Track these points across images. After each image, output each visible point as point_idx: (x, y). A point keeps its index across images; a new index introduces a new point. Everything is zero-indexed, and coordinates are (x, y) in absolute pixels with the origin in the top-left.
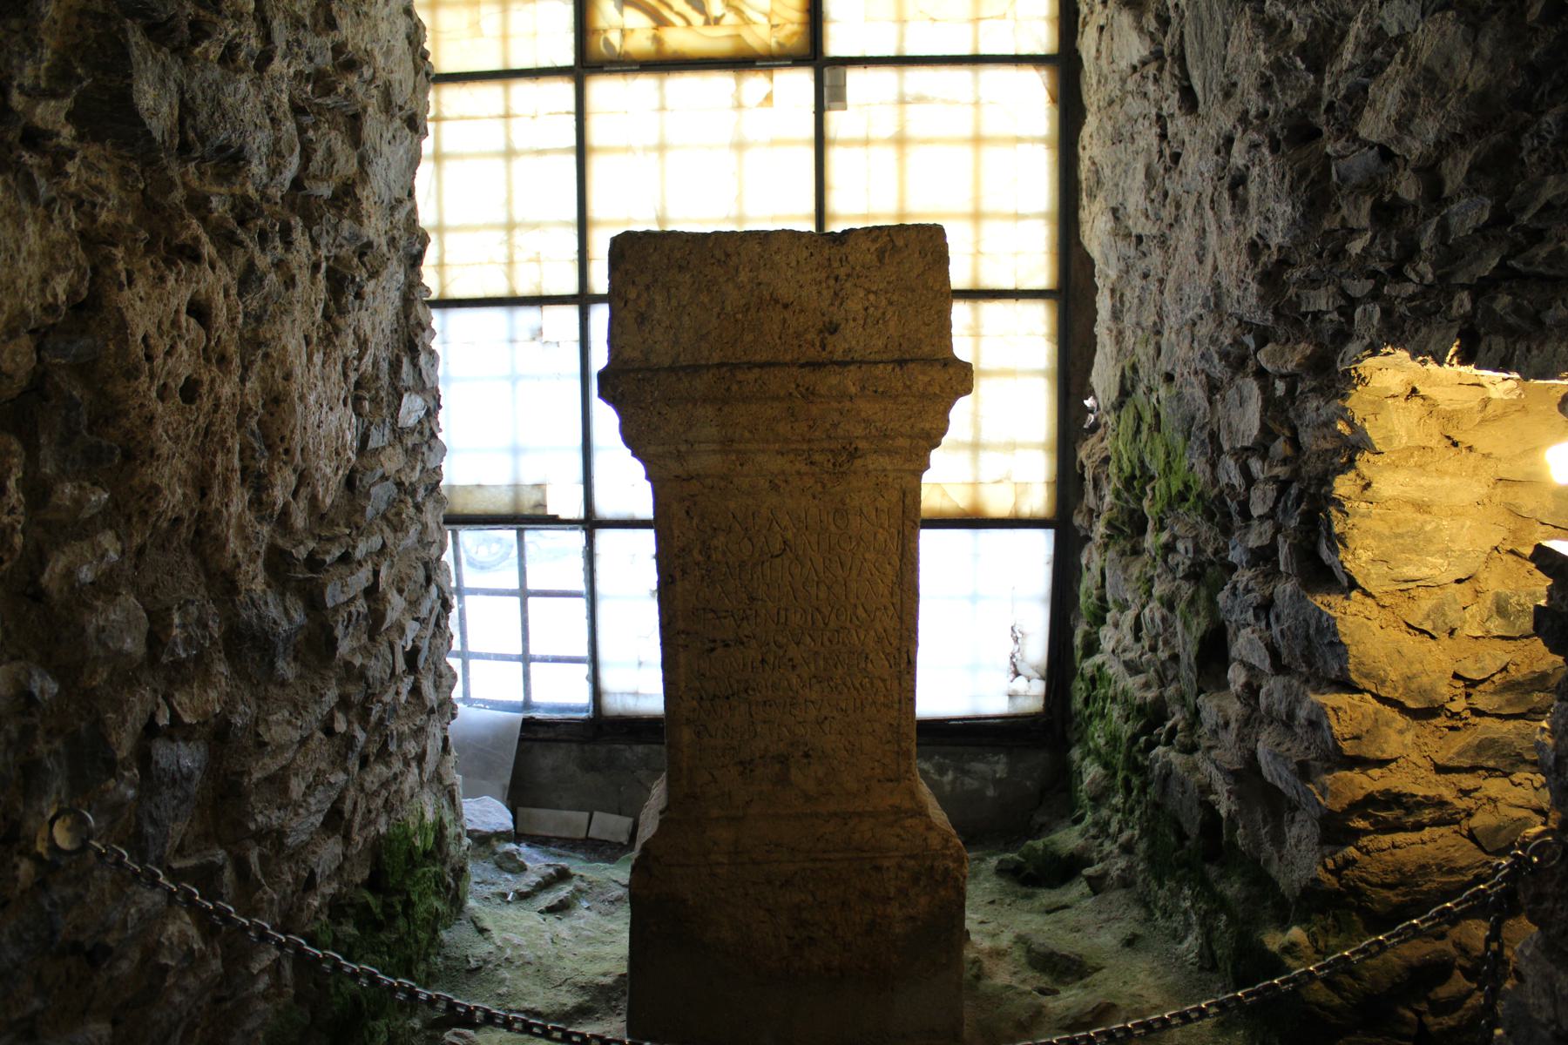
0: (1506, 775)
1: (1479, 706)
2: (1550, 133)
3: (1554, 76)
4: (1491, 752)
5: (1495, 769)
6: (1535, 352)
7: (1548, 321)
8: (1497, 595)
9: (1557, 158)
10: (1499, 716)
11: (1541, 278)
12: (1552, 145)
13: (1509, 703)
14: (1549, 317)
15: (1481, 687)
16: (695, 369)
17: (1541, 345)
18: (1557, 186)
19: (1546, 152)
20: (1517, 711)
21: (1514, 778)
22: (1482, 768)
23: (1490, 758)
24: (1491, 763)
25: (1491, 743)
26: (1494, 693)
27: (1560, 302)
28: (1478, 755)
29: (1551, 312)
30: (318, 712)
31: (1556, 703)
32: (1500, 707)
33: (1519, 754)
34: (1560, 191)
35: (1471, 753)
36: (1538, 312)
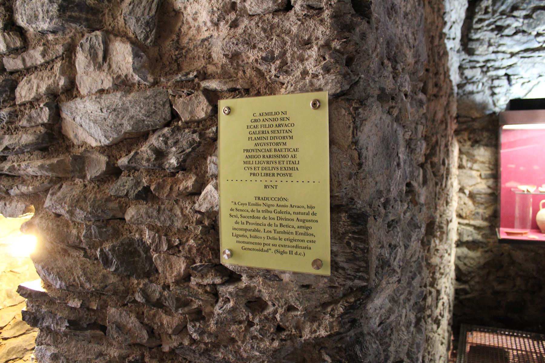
0: (21, 359)
1: (6, 336)
2: (5, 118)
3: (4, 95)
4: (13, 353)
5: (16, 358)
6: (8, 206)
7: (12, 194)
8: (7, 291)
9: (8, 128)
10: (15, 337)
11: (7, 176)
12: (6, 123)
13: (18, 330)
14: (12, 192)
15: (5, 328)
16: (140, 136)
17: (11, 202)
18: (9, 140)
19: (4, 126)
20: (22, 333)
21: (24, 359)
22: (10, 360)
23: (13, 355)
24: (14, 357)
25: (13, 348)
26: (12, 328)
27: (16, 187)
28: (8, 355)
29: (13, 190)
30: (345, 241)
31: (36, 347)
32: (15, 334)
33: (25, 349)
34: (11, 142)
35: (5, 356)
36: (7, 190)
